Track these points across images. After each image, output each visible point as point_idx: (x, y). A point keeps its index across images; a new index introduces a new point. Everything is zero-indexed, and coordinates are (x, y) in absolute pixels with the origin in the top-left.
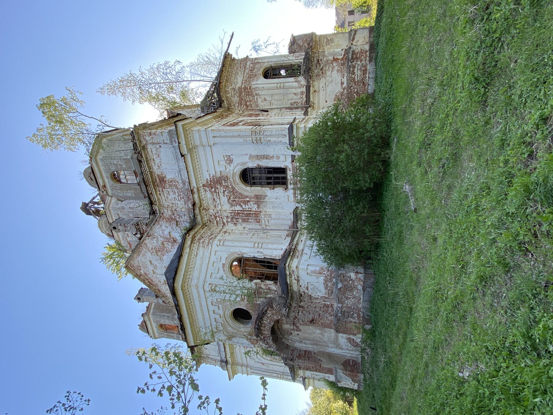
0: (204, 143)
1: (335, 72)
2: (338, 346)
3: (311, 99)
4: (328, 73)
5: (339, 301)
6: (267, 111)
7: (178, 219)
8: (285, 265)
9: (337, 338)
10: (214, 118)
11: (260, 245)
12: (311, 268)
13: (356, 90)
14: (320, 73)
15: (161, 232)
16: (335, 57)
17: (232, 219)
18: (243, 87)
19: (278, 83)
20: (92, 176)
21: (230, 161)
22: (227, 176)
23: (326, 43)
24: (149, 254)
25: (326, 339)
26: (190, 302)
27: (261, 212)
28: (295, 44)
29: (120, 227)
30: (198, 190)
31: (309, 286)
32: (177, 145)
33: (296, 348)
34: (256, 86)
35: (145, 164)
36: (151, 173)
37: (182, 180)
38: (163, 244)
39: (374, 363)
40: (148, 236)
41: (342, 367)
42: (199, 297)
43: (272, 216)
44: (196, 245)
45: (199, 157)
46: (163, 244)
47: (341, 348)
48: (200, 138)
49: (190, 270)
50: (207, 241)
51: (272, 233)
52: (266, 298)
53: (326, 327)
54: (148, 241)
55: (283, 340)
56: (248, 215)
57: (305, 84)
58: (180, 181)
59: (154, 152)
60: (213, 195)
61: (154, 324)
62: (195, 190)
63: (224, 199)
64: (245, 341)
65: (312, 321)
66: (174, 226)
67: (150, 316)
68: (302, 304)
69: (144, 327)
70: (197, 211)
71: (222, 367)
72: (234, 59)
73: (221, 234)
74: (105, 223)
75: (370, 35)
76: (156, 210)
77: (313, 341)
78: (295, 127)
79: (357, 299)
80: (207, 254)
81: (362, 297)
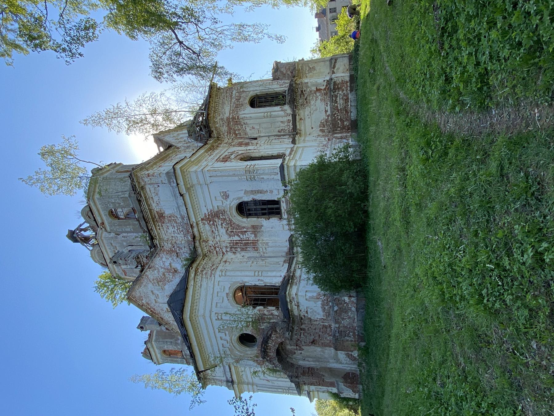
0: (201, 183)
1: (319, 101)
2: (338, 361)
3: (298, 127)
4: (312, 102)
5: (336, 322)
6: (256, 139)
7: (178, 251)
8: (285, 293)
9: (336, 355)
10: (206, 152)
11: (260, 273)
12: (309, 295)
13: (339, 117)
14: (305, 103)
15: (162, 264)
16: (318, 88)
17: (231, 248)
18: (231, 117)
19: (264, 113)
20: (90, 214)
21: (226, 196)
22: (224, 210)
23: (308, 71)
24: (150, 285)
25: (326, 356)
26: (198, 331)
27: (258, 240)
28: (279, 70)
29: (120, 261)
30: (197, 224)
31: (309, 310)
32: (175, 184)
33: (300, 366)
34: (244, 115)
35: (144, 203)
36: (150, 210)
37: (181, 215)
38: (164, 274)
39: (369, 375)
40: (149, 268)
41: (342, 380)
42: (207, 326)
43: (269, 244)
44: (199, 277)
45: (197, 194)
46: (164, 274)
47: (341, 363)
48: (197, 178)
49: (196, 301)
50: (209, 272)
51: (270, 259)
52: (269, 323)
53: (325, 346)
54: (149, 274)
55: (288, 360)
56: (246, 244)
57: (291, 113)
58: (179, 216)
59: (153, 191)
60: (211, 228)
61: (157, 351)
62: (195, 224)
63: (223, 231)
64: (251, 363)
65: (313, 342)
66: (175, 258)
67: (153, 343)
68: (303, 326)
69: (147, 354)
70: (197, 244)
71: (229, 387)
72: (219, 89)
73: (222, 264)
74: (98, 253)
75: (350, 62)
76: (157, 244)
77: (314, 358)
78: (285, 167)
79: (352, 319)
80: (211, 284)
81: (356, 317)
